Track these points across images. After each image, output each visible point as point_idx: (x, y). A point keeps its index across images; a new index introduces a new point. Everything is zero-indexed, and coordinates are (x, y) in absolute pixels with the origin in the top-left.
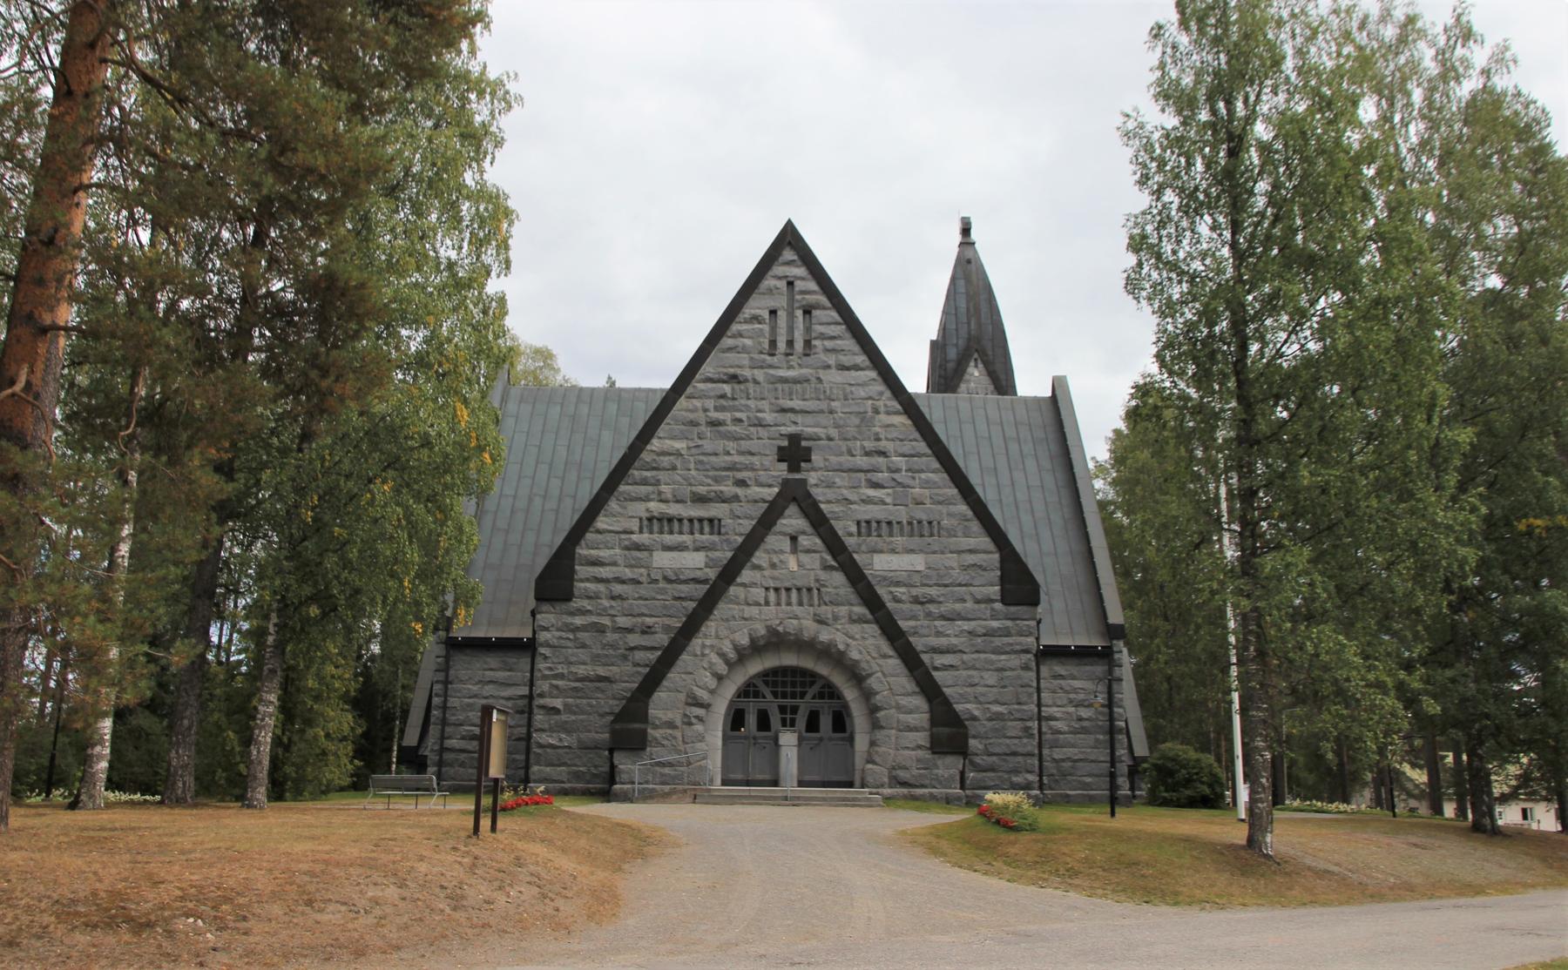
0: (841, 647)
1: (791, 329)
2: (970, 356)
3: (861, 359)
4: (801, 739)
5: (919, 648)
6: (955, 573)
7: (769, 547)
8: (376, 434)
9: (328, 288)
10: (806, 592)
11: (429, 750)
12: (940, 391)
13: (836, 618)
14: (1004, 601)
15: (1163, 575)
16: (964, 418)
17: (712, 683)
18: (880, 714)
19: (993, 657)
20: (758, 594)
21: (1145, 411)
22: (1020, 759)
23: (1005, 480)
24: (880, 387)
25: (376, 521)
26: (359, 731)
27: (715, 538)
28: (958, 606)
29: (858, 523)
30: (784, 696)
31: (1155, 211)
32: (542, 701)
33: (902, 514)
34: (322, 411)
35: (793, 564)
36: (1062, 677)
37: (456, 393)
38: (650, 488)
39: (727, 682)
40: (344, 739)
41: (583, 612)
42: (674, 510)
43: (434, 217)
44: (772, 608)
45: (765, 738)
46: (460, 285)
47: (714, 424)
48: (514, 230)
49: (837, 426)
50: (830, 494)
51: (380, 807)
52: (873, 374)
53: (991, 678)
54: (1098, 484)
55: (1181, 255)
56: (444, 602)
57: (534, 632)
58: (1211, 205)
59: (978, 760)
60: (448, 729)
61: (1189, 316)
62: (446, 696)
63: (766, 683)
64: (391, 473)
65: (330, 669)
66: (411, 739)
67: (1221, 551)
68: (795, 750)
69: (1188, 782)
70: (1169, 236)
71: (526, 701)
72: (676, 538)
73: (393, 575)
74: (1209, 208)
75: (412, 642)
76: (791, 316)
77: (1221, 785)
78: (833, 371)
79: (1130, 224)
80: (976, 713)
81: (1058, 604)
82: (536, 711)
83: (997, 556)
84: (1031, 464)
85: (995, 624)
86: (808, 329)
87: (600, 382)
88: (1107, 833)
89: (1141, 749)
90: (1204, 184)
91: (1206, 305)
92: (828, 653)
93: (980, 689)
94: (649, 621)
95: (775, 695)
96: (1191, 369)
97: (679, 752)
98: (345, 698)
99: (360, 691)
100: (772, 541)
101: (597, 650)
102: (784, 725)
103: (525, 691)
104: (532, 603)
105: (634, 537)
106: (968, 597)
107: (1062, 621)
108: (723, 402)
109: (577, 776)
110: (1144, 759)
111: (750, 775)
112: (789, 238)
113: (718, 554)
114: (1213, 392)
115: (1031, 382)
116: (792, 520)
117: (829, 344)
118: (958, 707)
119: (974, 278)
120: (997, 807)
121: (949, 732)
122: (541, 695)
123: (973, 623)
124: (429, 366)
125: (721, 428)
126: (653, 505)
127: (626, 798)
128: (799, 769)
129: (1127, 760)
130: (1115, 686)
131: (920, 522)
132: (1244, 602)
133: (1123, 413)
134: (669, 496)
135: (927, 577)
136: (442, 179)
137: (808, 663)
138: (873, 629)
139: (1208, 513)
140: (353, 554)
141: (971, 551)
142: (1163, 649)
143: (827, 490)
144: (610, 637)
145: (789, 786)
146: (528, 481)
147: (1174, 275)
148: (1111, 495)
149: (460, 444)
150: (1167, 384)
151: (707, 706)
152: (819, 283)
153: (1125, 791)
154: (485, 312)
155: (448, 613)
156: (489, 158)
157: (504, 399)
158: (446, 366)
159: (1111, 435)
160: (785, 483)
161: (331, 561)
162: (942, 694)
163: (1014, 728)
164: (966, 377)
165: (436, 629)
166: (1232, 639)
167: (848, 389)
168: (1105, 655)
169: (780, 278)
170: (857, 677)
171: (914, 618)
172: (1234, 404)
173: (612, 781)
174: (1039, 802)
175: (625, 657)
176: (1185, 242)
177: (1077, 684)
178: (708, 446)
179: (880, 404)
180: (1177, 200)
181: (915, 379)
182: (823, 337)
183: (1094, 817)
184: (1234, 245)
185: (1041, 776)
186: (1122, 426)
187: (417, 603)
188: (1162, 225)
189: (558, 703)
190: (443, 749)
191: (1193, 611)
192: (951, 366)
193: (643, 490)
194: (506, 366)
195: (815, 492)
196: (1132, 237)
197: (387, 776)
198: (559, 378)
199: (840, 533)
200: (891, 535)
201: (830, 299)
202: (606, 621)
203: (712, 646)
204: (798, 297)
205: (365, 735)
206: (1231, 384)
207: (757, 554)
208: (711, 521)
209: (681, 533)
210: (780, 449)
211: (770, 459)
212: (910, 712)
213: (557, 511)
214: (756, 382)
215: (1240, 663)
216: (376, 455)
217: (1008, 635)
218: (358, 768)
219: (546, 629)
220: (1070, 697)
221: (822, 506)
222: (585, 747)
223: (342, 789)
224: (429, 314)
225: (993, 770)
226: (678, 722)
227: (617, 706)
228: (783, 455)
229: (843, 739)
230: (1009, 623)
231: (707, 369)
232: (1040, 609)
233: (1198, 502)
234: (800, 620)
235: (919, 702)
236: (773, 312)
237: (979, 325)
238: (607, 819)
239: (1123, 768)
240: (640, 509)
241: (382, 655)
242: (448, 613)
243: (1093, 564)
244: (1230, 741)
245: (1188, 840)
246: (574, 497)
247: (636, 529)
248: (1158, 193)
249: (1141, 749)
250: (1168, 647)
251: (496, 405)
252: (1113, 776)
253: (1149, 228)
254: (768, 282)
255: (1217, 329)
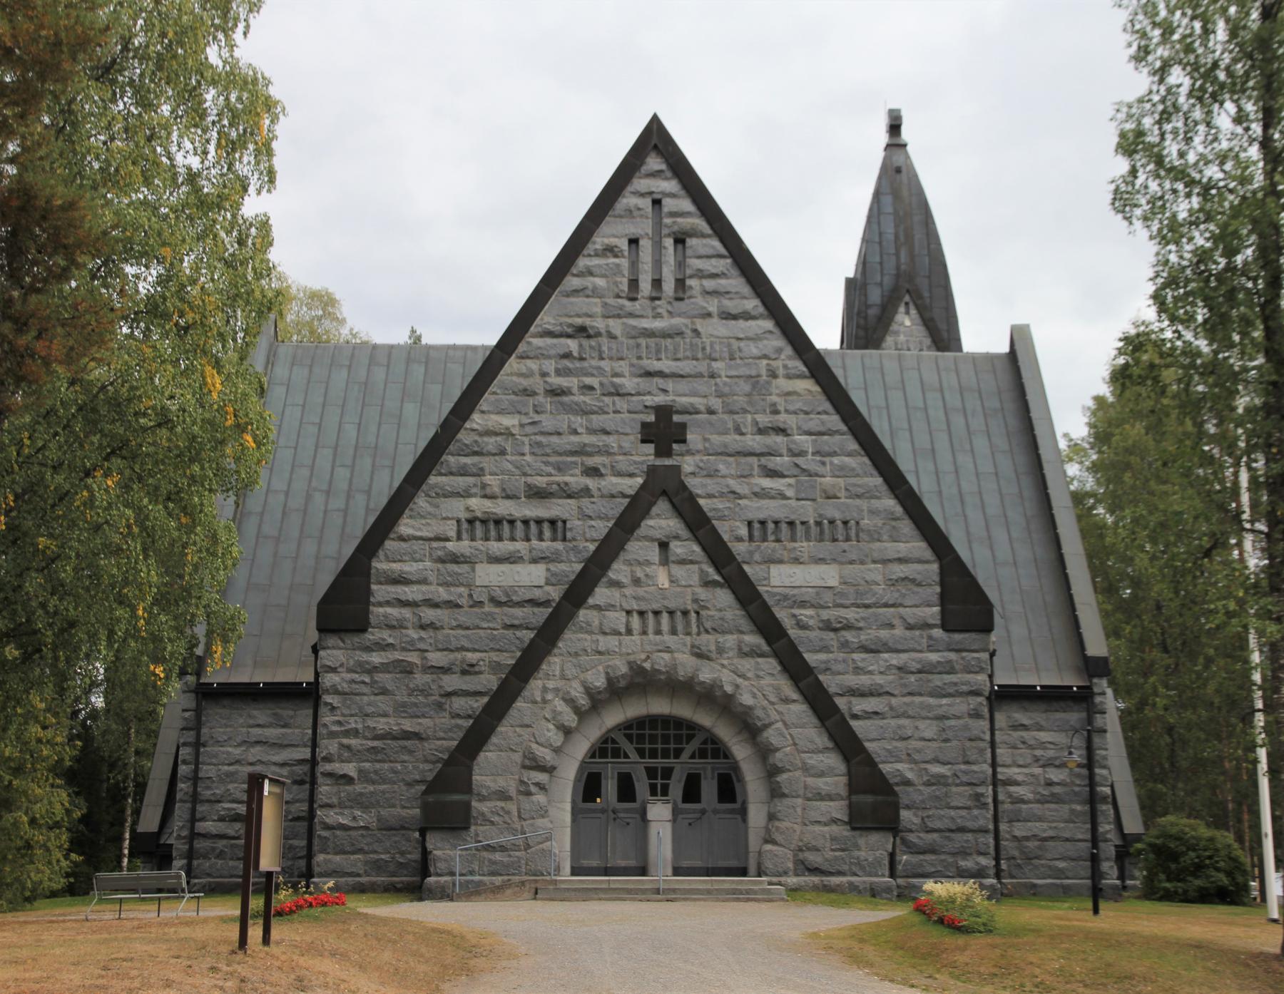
0: (729, 689)
1: (658, 264)
2: (900, 299)
3: (753, 304)
4: (676, 812)
5: (832, 690)
6: (879, 589)
7: (630, 557)
8: (94, 410)
9: (22, 209)
10: (680, 617)
11: (175, 837)
12: (857, 347)
13: (721, 650)
14: (945, 627)
15: (1160, 589)
16: (889, 383)
17: (557, 738)
18: (782, 778)
19: (931, 701)
20: (617, 619)
21: (1136, 371)
22: (970, 836)
23: (946, 464)
24: (778, 342)
25: (97, 528)
26: (77, 814)
27: (559, 545)
28: (884, 634)
29: (750, 524)
30: (653, 754)
31: (1156, 98)
32: (328, 767)
33: (808, 512)
34: (19, 380)
35: (663, 579)
36: (1024, 727)
37: (204, 352)
38: (471, 480)
39: (577, 737)
40: (57, 825)
41: (383, 647)
42: (503, 508)
43: (166, 109)
44: (636, 638)
45: (627, 811)
46: (205, 205)
47: (555, 392)
48: (279, 129)
49: (720, 395)
50: (712, 485)
51: (108, 916)
52: (768, 324)
53: (928, 729)
54: (1073, 470)
55: (1192, 158)
56: (193, 636)
57: (317, 674)
58: (1236, 88)
59: (912, 837)
60: (200, 808)
61: (1200, 241)
62: (197, 763)
63: (629, 737)
64: (117, 462)
65: (35, 730)
66: (149, 822)
67: (1242, 559)
68: (669, 826)
69: (1198, 868)
70: (1175, 132)
71: (306, 768)
72: (506, 547)
73: (122, 601)
74: (1233, 92)
75: (152, 693)
76: (658, 246)
77: (1245, 873)
78: (715, 320)
79: (1121, 116)
80: (910, 775)
81: (1018, 630)
82: (320, 780)
83: (935, 567)
84: (981, 443)
85: (934, 657)
86: (681, 264)
87: (399, 337)
88: (1088, 935)
89: (1133, 824)
90: (1227, 58)
91: (1224, 227)
92: (711, 697)
93: (914, 744)
94: (471, 657)
95: (641, 753)
96: (1201, 314)
97: (514, 832)
98: (56, 769)
99: (77, 760)
100: (638, 548)
101: (402, 697)
102: (653, 793)
103: (305, 753)
104: (314, 636)
105: (450, 545)
106: (896, 622)
107: (1023, 650)
108: (567, 363)
109: (378, 867)
110: (1137, 838)
111: (611, 862)
112: (655, 141)
113: (562, 567)
114: (1232, 345)
115: (981, 334)
116: (662, 521)
117: (709, 284)
118: (886, 768)
119: (905, 193)
120: (940, 901)
121: (874, 800)
122: (328, 759)
123: (904, 656)
124: (166, 316)
125: (565, 399)
126: (474, 502)
127: (443, 895)
128: (674, 851)
129: (1114, 838)
130: (1097, 740)
131: (831, 522)
132: (1272, 628)
133: (1106, 374)
134: (497, 490)
135: (842, 594)
136: (175, 56)
137: (683, 710)
138: (771, 664)
139: (1223, 508)
140: (66, 572)
141: (901, 560)
142: (1161, 690)
143: (708, 481)
144: (420, 679)
145: (662, 875)
146: (305, 472)
147: (1180, 186)
148: (1090, 483)
149: (211, 423)
150: (1168, 334)
151: (550, 770)
152: (695, 201)
153: (1111, 880)
154: (241, 242)
155: (199, 651)
156: (241, 26)
157: (270, 361)
158: (190, 317)
159: (1091, 404)
160: (652, 471)
161: (34, 583)
162: (864, 750)
163: (960, 795)
164: (894, 327)
165: (183, 673)
166: (1257, 677)
167: (735, 344)
168: (1084, 698)
169: (642, 195)
170: (750, 728)
171: (825, 649)
172: (1260, 361)
173: (425, 873)
174: (997, 895)
175: (440, 706)
176: (1197, 140)
177: (1044, 736)
178: (548, 422)
179: (778, 364)
180: (1187, 82)
181: (825, 327)
182: (700, 274)
183: (1071, 914)
184: (1266, 143)
185: (997, 859)
186: (1105, 390)
187: (156, 639)
188: (1165, 116)
189: (350, 769)
190: (194, 835)
191: (1204, 640)
192: (873, 312)
193: (462, 482)
194: (272, 316)
195: (692, 483)
196: (1123, 135)
197: (116, 874)
198: (345, 331)
199: (726, 537)
200: (793, 539)
201: (709, 222)
202: (413, 658)
203: (557, 690)
204: (667, 221)
205: (84, 820)
206: (1257, 334)
207: (615, 566)
208: (553, 522)
209: (513, 539)
210: (644, 425)
211: (631, 440)
212: (822, 774)
213: (345, 512)
214: (612, 337)
215: (1268, 709)
216: (95, 439)
217: (952, 671)
218: (75, 864)
219: (333, 670)
220: (1035, 754)
221: (702, 502)
222: (387, 828)
223: (53, 894)
224: (164, 244)
225: (933, 852)
226: (513, 792)
227: (430, 771)
228: (649, 434)
229: (732, 811)
230: (952, 656)
231: (546, 319)
232: (993, 637)
233: (1209, 493)
234: (673, 653)
235: (833, 761)
236: (634, 242)
237: (912, 256)
238: (419, 923)
239: (1108, 850)
240: (457, 508)
241: (107, 711)
242: (199, 651)
243: (1066, 577)
244: (1256, 814)
245: (1198, 946)
246: (368, 493)
247: (453, 534)
248: (1162, 72)
249: (1133, 824)
250: (1167, 687)
251: (259, 368)
252: (1095, 859)
253: (1147, 122)
254: (627, 200)
255: (1239, 259)
